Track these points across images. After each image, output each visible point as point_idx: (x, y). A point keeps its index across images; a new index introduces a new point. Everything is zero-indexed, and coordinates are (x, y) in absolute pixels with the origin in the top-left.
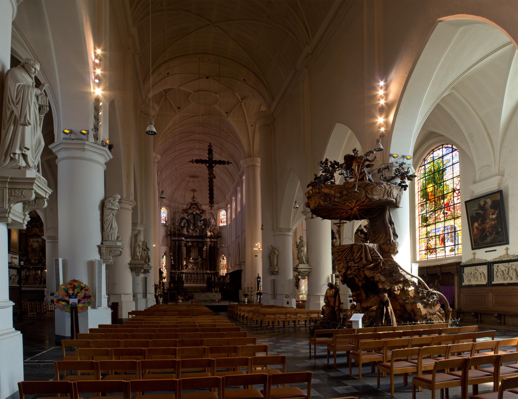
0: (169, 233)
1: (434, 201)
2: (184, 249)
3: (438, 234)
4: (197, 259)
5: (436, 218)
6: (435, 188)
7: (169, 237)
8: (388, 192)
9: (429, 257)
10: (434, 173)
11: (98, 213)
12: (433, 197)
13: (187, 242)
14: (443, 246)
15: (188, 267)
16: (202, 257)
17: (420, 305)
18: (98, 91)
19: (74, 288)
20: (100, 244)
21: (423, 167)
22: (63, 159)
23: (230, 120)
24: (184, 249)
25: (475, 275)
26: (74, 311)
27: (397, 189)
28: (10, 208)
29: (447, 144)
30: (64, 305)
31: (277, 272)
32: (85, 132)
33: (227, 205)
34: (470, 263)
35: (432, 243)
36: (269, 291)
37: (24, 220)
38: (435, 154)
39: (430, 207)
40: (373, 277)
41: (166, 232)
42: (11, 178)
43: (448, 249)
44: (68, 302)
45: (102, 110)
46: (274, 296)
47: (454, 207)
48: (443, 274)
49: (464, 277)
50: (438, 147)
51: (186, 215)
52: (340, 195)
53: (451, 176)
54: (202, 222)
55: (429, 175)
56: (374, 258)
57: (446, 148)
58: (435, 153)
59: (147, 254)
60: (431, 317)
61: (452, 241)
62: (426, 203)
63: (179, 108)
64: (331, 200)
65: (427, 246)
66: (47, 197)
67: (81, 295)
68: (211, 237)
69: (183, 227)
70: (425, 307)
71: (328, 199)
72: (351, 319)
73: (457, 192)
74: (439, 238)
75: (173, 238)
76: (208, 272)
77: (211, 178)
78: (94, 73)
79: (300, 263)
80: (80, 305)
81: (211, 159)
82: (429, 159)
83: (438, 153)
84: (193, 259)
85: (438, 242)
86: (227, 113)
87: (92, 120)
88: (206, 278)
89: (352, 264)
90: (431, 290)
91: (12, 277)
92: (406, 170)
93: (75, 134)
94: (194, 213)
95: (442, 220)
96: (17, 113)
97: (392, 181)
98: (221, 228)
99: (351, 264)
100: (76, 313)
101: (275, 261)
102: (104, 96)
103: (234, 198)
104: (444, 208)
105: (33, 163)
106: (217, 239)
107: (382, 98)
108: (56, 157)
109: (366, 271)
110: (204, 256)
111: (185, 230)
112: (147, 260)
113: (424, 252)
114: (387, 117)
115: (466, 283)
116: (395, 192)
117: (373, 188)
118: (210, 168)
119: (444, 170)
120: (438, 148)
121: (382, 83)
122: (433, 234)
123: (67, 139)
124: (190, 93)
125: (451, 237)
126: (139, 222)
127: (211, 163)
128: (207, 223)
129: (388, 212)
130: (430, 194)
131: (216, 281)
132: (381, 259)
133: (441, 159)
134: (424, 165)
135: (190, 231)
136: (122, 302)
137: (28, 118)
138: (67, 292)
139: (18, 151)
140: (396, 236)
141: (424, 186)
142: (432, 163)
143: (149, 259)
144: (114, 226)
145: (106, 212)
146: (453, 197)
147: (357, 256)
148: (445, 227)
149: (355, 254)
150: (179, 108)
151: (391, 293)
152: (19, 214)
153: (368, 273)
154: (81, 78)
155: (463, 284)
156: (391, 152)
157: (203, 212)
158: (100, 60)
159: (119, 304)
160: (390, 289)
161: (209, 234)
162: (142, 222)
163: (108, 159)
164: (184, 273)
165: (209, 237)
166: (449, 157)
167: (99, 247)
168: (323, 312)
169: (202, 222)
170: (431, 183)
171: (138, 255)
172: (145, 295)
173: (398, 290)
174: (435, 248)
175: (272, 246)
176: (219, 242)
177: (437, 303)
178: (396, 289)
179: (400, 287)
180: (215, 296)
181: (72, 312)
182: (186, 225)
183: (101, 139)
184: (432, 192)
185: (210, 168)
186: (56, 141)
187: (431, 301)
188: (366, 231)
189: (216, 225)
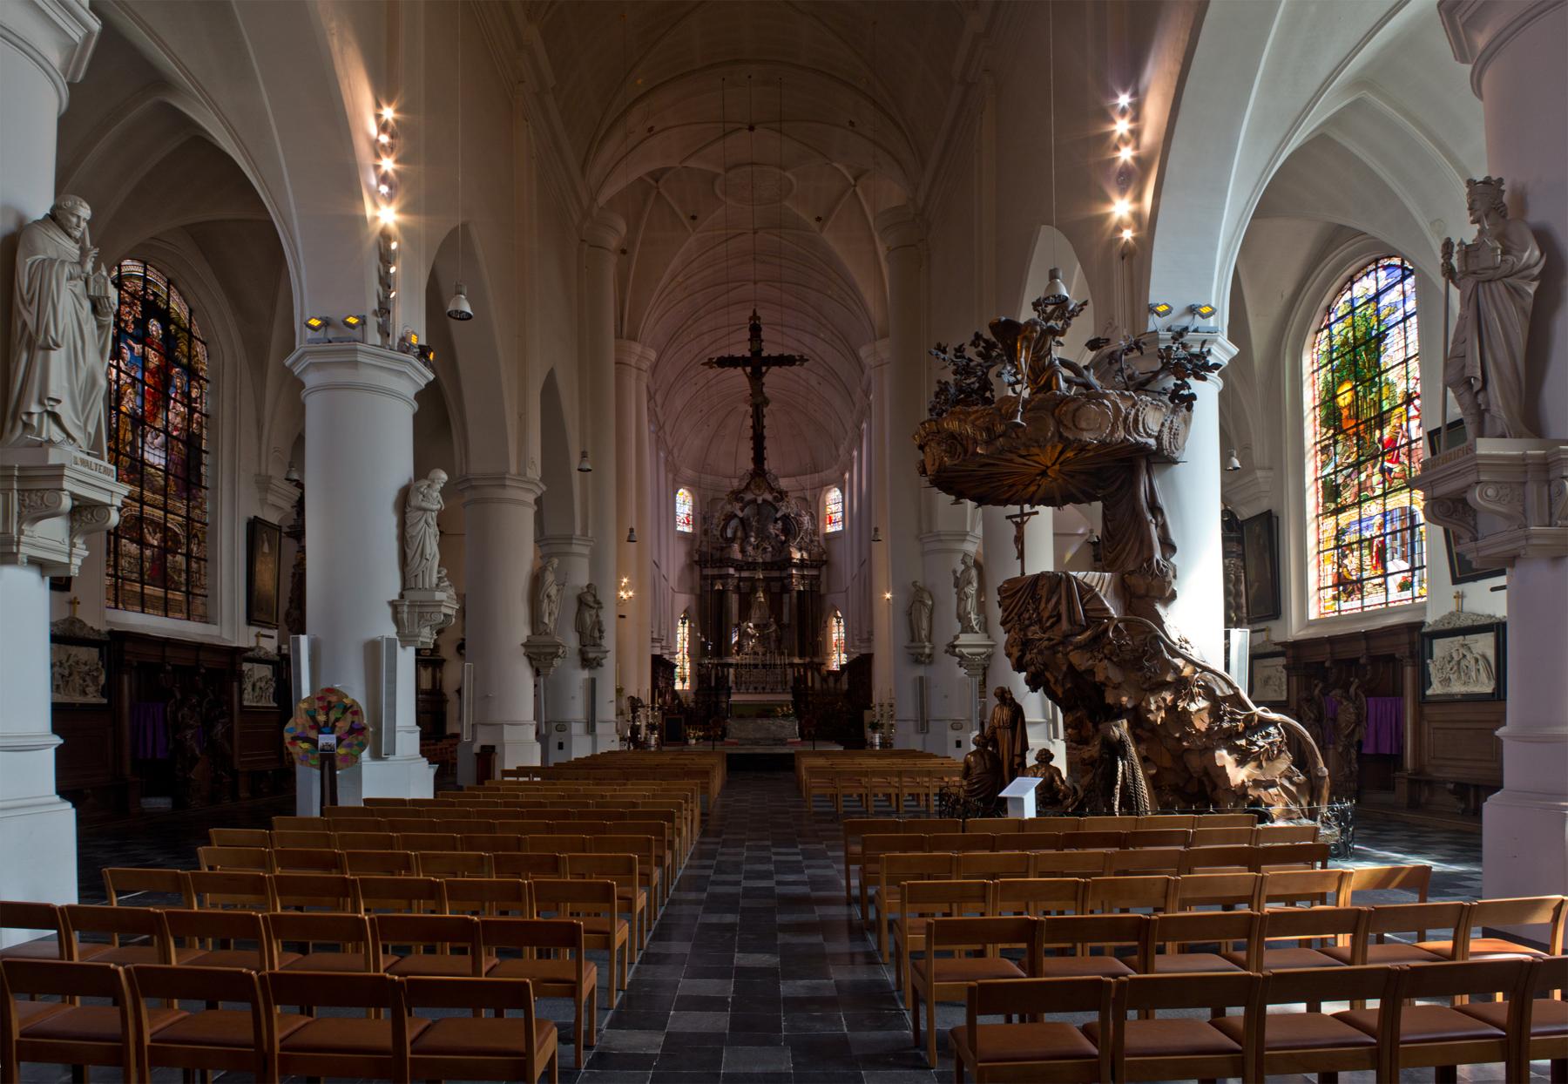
1: (1357, 434)
2: (734, 601)
3: (1367, 534)
4: (766, 626)
5: (1361, 487)
6: (1357, 393)
7: (697, 568)
8: (1126, 418)
9: (1344, 606)
10: (1354, 349)
11: (391, 522)
12: (1353, 423)
13: (740, 579)
14: (1379, 572)
15: (745, 638)
16: (778, 621)
17: (1224, 758)
18: (386, 215)
19: (328, 708)
20: (396, 597)
21: (1326, 332)
22: (317, 389)
23: (828, 237)
24: (734, 601)
25: (1463, 663)
26: (328, 762)
27: (1158, 408)
28: (21, 532)
29: (1390, 257)
30: (306, 751)
31: (930, 656)
32: (353, 320)
34: (1447, 627)
35: (1352, 562)
36: (907, 709)
37: (70, 555)
38: (1358, 289)
39: (1345, 453)
40: (1091, 672)
41: (689, 554)
42: (20, 469)
43: (1393, 582)
44: (315, 742)
45: (399, 261)
46: (923, 724)
47: (1410, 450)
48: (1374, 660)
49: (1432, 668)
50: (1366, 266)
52: (989, 435)
53: (1400, 356)
54: (780, 524)
55: (1343, 355)
56: (1091, 614)
57: (1385, 268)
58: (1356, 287)
60: (1262, 792)
61: (1404, 557)
62: (1336, 442)
63: (694, 218)
64: (966, 451)
65: (1339, 574)
67: (343, 726)
68: (802, 564)
69: (733, 540)
70: (1241, 763)
71: (959, 449)
72: (1002, 794)
73: (1417, 402)
74: (1370, 547)
75: (709, 572)
76: (797, 660)
77: (759, 405)
78: (377, 167)
79: (964, 631)
80: (341, 751)
81: (756, 353)
82: (1341, 307)
83: (1365, 287)
84: (756, 626)
85: (1367, 560)
86: (819, 219)
87: (375, 286)
88: (790, 677)
90: (1258, 710)
92: (1196, 349)
93: (336, 326)
95: (1379, 492)
96: (31, 325)
98: (831, 537)
100: (333, 769)
101: (925, 624)
102: (401, 227)
103: (855, 453)
104: (1383, 454)
106: (818, 567)
107: (1126, 143)
108: (302, 385)
109: (1098, 652)
110: (786, 619)
111: (736, 547)
112: (597, 634)
113: (1330, 592)
114: (1138, 198)
115: (1436, 689)
116: (1153, 420)
117: (1077, 409)
118: (756, 378)
119: (1381, 337)
120: (1363, 271)
121: (1124, 100)
122: (1354, 538)
123: (317, 341)
124: (718, 175)
125: (1402, 545)
126: (578, 532)
127: (756, 364)
128: (790, 527)
129: (1144, 479)
130: (1345, 413)
131: (817, 685)
132: (1111, 618)
133: (1372, 305)
134: (1328, 326)
135: (750, 549)
136: (503, 745)
137: (53, 333)
138: (313, 718)
140: (1169, 547)
142: (1349, 320)
143: (601, 631)
144: (428, 551)
145: (412, 516)
146: (1408, 420)
147: (1047, 609)
148: (1384, 514)
149: (1043, 605)
150: (694, 218)
151: (1138, 719)
153: (1080, 661)
154: (348, 183)
155: (1429, 692)
156: (1152, 301)
157: (782, 495)
158: (392, 137)
159: (498, 750)
160: (1136, 708)
161: (797, 555)
162: (585, 533)
163: (423, 383)
164: (730, 665)
165: (795, 566)
166: (1393, 296)
167: (394, 605)
168: (967, 771)
169: (780, 524)
170: (1348, 380)
172: (591, 727)
173: (1159, 708)
174: (1361, 580)
176: (823, 578)
177: (1280, 752)
178: (1153, 707)
179: (1164, 700)
180: (783, 727)
181: (322, 769)
182: (739, 534)
183: (398, 330)
184: (1349, 406)
187: (1261, 743)
189: (815, 532)
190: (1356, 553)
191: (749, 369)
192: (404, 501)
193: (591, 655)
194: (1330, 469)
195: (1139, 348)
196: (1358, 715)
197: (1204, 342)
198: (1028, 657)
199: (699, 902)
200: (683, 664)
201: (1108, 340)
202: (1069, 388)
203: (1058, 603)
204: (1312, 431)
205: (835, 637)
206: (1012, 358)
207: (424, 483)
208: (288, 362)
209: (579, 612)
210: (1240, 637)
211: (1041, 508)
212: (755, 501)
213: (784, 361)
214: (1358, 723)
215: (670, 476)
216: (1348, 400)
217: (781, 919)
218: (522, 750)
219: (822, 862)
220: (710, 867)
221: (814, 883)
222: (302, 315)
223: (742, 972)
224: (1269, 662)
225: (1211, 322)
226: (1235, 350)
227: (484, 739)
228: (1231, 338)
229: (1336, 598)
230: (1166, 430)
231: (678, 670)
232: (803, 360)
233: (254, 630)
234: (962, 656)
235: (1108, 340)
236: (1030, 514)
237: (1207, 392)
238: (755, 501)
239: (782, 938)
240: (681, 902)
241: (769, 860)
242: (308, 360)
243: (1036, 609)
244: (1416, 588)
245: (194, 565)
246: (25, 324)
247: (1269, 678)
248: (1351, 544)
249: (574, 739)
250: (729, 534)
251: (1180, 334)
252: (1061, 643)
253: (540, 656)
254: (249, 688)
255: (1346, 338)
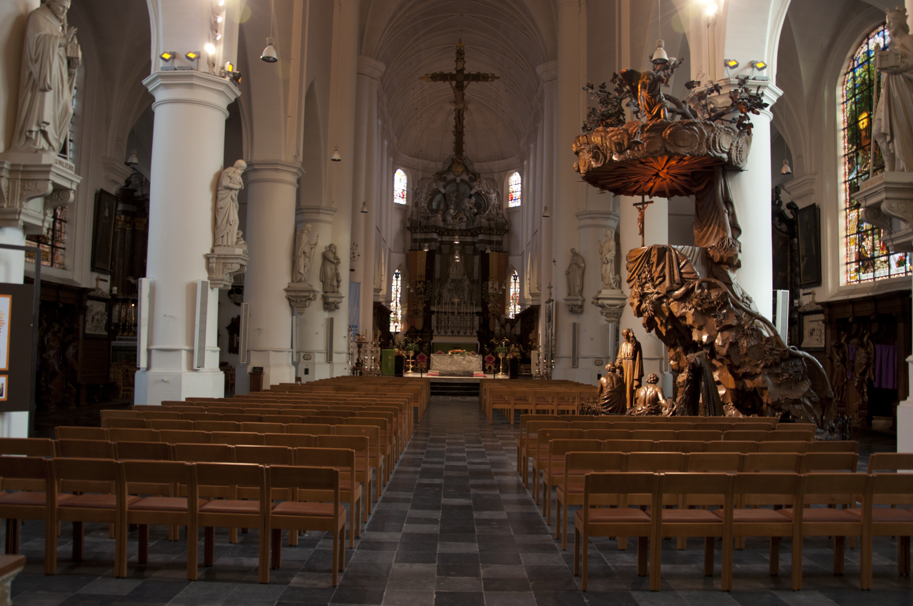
0: (408, 225)
7: (409, 233)
8: (708, 139)
9: (864, 276)
13: (442, 242)
20: (209, 252)
27: (728, 133)
28: (21, 206)
33: (522, 162)
35: (867, 244)
37: (43, 221)
41: (403, 222)
42: (24, 166)
50: (877, 27)
51: (442, 184)
54: (473, 199)
56: (685, 276)
59: (336, 269)
62: (857, 155)
66: (74, 187)
69: (436, 211)
75: (419, 236)
81: (460, 71)
82: (861, 54)
85: (877, 242)
89: (649, 288)
91: (96, 317)
92: (754, 92)
94: (458, 180)
96: (35, 75)
97: (723, 118)
99: (649, 288)
105: (58, 141)
108: (152, 99)
111: (439, 216)
112: (335, 283)
113: (854, 266)
116: (725, 142)
118: (460, 88)
127: (460, 80)
128: (481, 203)
130: (863, 134)
134: (853, 70)
135: (449, 218)
136: (269, 366)
137: (48, 81)
139: (35, 128)
140: (737, 230)
141: (852, 118)
142: (866, 66)
143: (338, 281)
144: (231, 219)
149: (654, 268)
152: (36, 214)
157: (475, 177)
159: (265, 370)
171: (302, 271)
172: (329, 359)
174: (873, 258)
175: (573, 251)
180: (471, 362)
182: (442, 206)
185: (460, 88)
186: (152, 72)
188: (791, 217)
189: (500, 207)
190: (870, 238)
191: (454, 83)
192: (217, 185)
193: (331, 300)
194: (853, 175)
195: (718, 91)
196: (868, 359)
197: (759, 87)
198: (644, 306)
199: (416, 473)
200: (397, 310)
201: (699, 83)
202: (673, 118)
203: (664, 268)
204: (842, 146)
205: (512, 291)
206: (634, 93)
207: (230, 170)
208: (145, 82)
209: (323, 265)
210: (783, 295)
211: (656, 199)
212: (455, 180)
213: (478, 77)
214: (868, 365)
215: (391, 159)
216: (865, 125)
217: (472, 482)
218: (280, 373)
219: (498, 452)
220: (423, 454)
221: (493, 464)
222: (157, 50)
223: (447, 508)
224: (814, 317)
225: (764, 73)
226: (780, 92)
227: (255, 362)
228: (779, 84)
229: (857, 271)
230: (734, 148)
231: (392, 315)
232: (494, 77)
233: (95, 275)
234: (602, 306)
235: (699, 83)
236: (647, 203)
237: (761, 123)
238: (455, 180)
239: (473, 491)
240: (404, 472)
241: (462, 451)
242: (159, 82)
243: (650, 271)
244: (908, 265)
245: (58, 225)
246: (31, 74)
247: (814, 330)
248: (867, 231)
249: (317, 367)
250: (434, 206)
251: (743, 82)
252: (665, 296)
253: (297, 300)
254: (90, 320)
255: (864, 78)
